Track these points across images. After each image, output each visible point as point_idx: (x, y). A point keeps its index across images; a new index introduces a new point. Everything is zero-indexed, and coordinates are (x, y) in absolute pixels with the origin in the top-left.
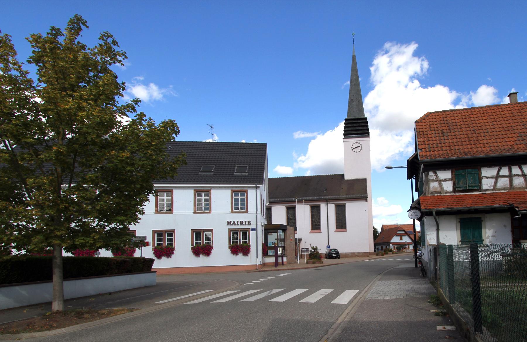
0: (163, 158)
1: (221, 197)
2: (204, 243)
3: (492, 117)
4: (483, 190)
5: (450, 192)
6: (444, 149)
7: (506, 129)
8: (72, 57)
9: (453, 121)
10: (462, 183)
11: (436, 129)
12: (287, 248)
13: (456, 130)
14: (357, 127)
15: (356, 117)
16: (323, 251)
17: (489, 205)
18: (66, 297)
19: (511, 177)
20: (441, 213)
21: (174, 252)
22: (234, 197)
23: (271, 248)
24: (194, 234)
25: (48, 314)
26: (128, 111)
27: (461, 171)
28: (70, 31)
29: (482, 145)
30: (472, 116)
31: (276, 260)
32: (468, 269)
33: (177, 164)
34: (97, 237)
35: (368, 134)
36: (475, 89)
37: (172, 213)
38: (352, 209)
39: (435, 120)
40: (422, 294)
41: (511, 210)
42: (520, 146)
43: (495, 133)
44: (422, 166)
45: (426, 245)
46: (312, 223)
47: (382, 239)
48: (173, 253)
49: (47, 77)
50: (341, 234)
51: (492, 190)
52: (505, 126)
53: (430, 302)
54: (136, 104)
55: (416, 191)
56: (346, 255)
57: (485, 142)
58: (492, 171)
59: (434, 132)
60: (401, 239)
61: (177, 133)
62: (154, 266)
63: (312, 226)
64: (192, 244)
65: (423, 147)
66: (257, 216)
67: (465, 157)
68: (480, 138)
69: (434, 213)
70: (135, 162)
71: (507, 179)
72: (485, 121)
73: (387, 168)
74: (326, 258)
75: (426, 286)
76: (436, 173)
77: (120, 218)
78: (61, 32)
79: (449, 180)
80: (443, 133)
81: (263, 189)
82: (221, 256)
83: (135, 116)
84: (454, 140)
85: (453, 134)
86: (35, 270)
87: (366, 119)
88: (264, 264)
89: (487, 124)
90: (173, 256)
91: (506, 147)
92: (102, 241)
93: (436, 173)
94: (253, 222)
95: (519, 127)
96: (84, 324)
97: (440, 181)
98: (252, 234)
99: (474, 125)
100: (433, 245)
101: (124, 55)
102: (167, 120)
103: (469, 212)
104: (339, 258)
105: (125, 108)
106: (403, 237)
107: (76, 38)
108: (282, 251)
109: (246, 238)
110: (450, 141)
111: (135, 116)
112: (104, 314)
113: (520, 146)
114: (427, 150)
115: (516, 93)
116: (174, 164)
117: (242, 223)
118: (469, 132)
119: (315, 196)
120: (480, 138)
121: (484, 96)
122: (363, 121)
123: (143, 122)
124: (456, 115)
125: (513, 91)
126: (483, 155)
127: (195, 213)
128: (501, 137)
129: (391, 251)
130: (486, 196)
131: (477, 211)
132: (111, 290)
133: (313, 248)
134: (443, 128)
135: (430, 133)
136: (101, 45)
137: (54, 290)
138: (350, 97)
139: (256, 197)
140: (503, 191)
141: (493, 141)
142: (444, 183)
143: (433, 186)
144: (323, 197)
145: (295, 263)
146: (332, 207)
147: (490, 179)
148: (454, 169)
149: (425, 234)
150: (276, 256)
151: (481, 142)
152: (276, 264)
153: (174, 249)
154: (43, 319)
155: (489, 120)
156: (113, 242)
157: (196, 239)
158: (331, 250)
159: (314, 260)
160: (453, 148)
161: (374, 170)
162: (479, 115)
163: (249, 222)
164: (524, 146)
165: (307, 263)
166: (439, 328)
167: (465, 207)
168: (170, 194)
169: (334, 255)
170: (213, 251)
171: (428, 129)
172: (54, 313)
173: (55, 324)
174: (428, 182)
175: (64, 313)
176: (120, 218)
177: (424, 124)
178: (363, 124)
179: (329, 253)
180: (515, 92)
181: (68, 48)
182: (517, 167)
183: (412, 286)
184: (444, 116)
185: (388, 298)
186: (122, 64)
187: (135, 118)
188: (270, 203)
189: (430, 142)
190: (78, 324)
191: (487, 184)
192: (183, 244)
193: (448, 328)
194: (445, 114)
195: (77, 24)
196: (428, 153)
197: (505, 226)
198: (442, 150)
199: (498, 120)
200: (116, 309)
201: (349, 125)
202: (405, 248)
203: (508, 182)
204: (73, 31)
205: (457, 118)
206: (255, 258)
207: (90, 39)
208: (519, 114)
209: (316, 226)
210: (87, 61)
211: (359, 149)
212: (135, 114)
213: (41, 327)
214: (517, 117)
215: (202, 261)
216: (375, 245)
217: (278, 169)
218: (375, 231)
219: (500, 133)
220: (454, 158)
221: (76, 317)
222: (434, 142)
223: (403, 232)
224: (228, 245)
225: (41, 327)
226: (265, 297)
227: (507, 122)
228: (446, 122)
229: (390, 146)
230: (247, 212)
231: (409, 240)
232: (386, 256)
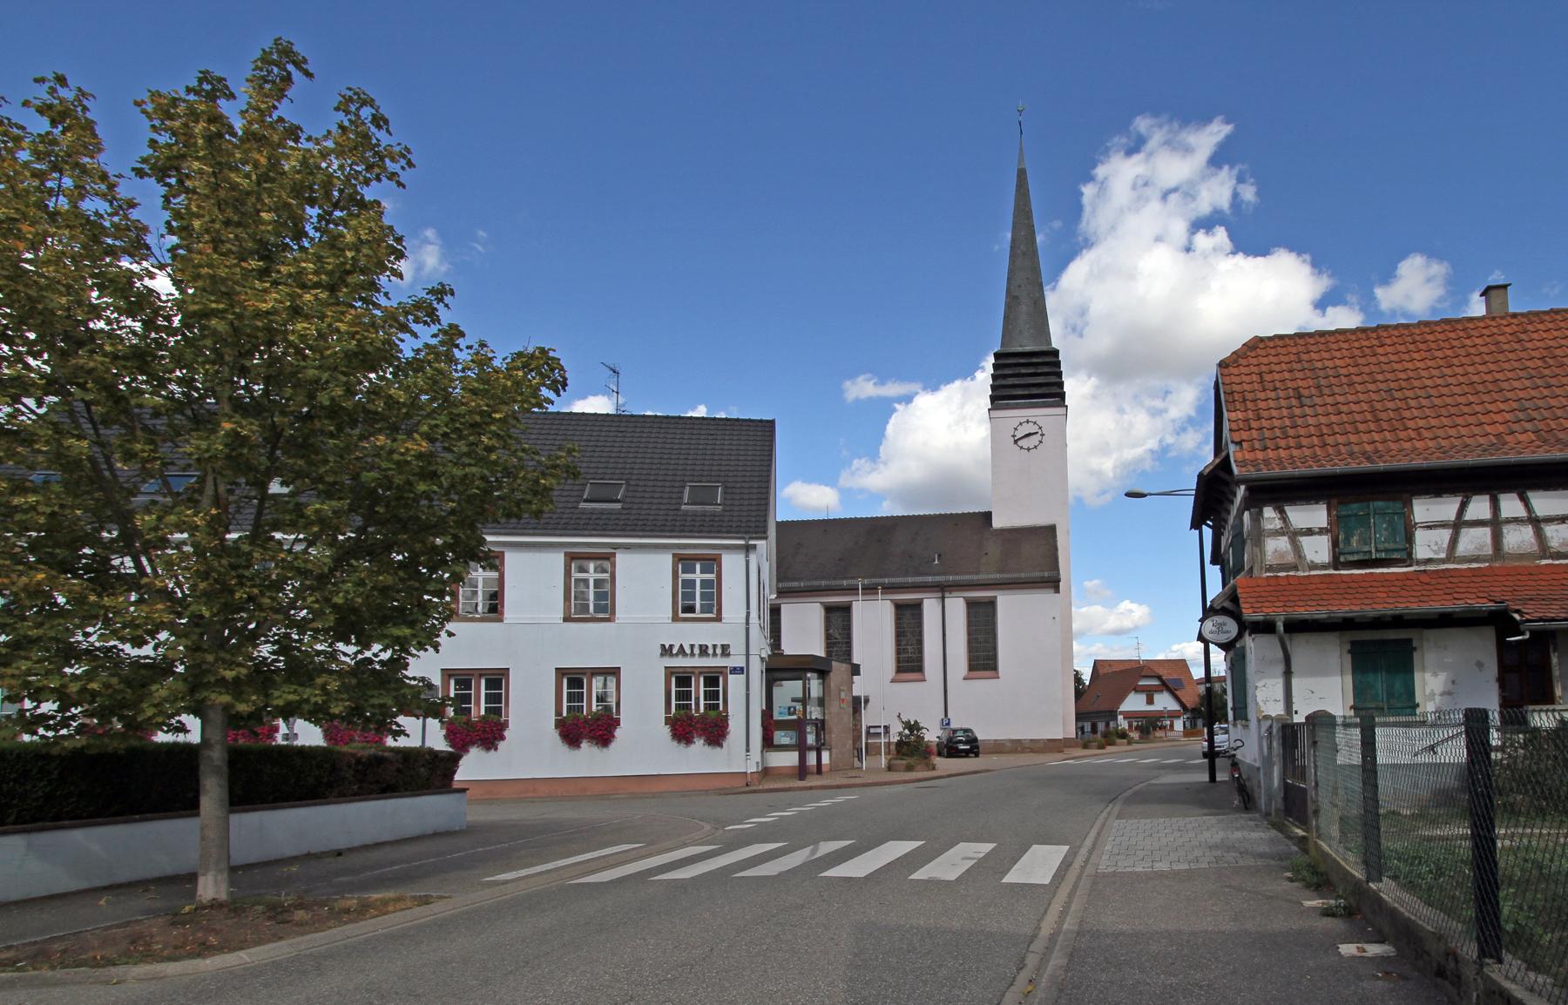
0: (520, 459)
1: (644, 575)
2: (594, 708)
3: (1439, 354)
4: (1419, 563)
5: (1324, 567)
6: (1304, 442)
7: (1480, 388)
8: (263, 161)
9: (1328, 363)
10: (1359, 542)
11: (1278, 385)
12: (830, 724)
13: (1337, 390)
14: (1028, 378)
15: (1028, 349)
16: (932, 735)
18: (233, 863)
19: (1496, 524)
20: (1298, 627)
21: (506, 733)
22: (683, 576)
23: (783, 725)
24: (565, 681)
25: (187, 909)
26: (417, 321)
27: (1355, 506)
28: (261, 87)
29: (1413, 434)
30: (1380, 350)
31: (802, 759)
33: (553, 476)
34: (334, 685)
35: (1062, 396)
36: (1388, 276)
37: (501, 620)
38: (1011, 608)
39: (1275, 360)
40: (1261, 856)
41: (1500, 621)
42: (1521, 438)
43: (1449, 400)
44: (1241, 491)
45: (1252, 715)
46: (898, 652)
47: (1101, 696)
48: (502, 738)
49: (207, 218)
50: (983, 686)
51: (1443, 561)
52: (1475, 378)
53: (1291, 880)
54: (441, 300)
55: (1213, 562)
56: (998, 748)
57: (1421, 423)
58: (1446, 508)
59: (1273, 395)
60: (1150, 701)
61: (560, 386)
62: (461, 775)
63: (898, 661)
64: (558, 712)
65: (1245, 435)
66: (747, 630)
67: (1366, 466)
68: (1407, 414)
69: (1280, 626)
70: (441, 469)
71: (1487, 531)
72: (1419, 364)
73: (1129, 495)
74: (940, 754)
76: (1282, 512)
77: (396, 632)
78: (227, 87)
79: (1321, 531)
80: (1299, 397)
81: (765, 548)
82: (644, 745)
83: (435, 336)
84: (1334, 418)
85: (1330, 400)
86: (121, 781)
87: (1056, 353)
88: (766, 772)
89: (1424, 373)
90: (502, 745)
91: (1482, 440)
92: (345, 696)
93: (1282, 512)
94: (737, 648)
95: (1516, 384)
96: (299, 939)
97: (1294, 535)
98: (735, 683)
99: (1389, 376)
100: (1278, 718)
101: (404, 157)
102: (530, 350)
103: (1378, 623)
104: (977, 755)
105: (407, 313)
106: (1157, 697)
107: (275, 108)
108: (818, 736)
109: (715, 695)
110: (1323, 420)
111: (435, 336)
112: (347, 911)
113: (1521, 438)
114: (1257, 445)
115: (1505, 287)
116: (544, 475)
117: (704, 651)
118: (1374, 397)
119: (906, 574)
120: (1407, 414)
121: (1414, 290)
122: (1047, 359)
123: (456, 351)
124: (1335, 346)
125: (1497, 278)
126: (1418, 462)
127: (566, 619)
128: (1466, 409)
129: (1123, 735)
130: (1425, 579)
131: (1398, 621)
132: (342, 843)
133: (908, 725)
134: (1300, 383)
135: (1262, 395)
136: (341, 127)
137: (203, 838)
138: (1008, 291)
139: (743, 574)
140: (1475, 565)
141: (1445, 421)
142: (1305, 541)
143: (1276, 547)
144: (930, 579)
145: (853, 768)
147: (1436, 530)
148: (1334, 501)
149: (1250, 685)
150: (802, 748)
151: (1411, 424)
152: (802, 771)
153: (505, 725)
154: (173, 924)
155: (1430, 363)
156: (376, 701)
157: (571, 698)
158: (955, 731)
159: (910, 761)
160: (1330, 440)
161: (1079, 500)
162: (1402, 348)
163: (725, 648)
165: (890, 768)
166: (1348, 949)
167: (1367, 608)
168: (607, 565)
169: (960, 746)
170: (618, 732)
171: (1256, 386)
172: (205, 908)
173: (212, 940)
174: (1259, 536)
175: (233, 907)
176: (396, 632)
177: (1243, 370)
178: (1046, 369)
179: (950, 740)
180: (1501, 283)
181: (254, 134)
182: (1514, 495)
183: (1221, 834)
184: (1301, 349)
185: (1163, 866)
186: (400, 184)
187: (434, 341)
188: (782, 593)
189: (1265, 423)
190: (281, 938)
191: (1428, 545)
192: (532, 710)
193: (1374, 950)
194: (1302, 342)
195: (279, 68)
196: (1260, 455)
197: (1480, 665)
198: (1300, 447)
199: (1455, 361)
200: (375, 896)
201: (1007, 371)
202: (1163, 728)
203: (1489, 540)
204: (268, 86)
205: (1338, 354)
206: (739, 754)
207: (312, 114)
208: (1516, 346)
209: (909, 662)
210: (311, 173)
211: (1034, 440)
212: (435, 329)
213: (176, 948)
214: (1511, 356)
215: (588, 762)
216: (1079, 717)
217: (803, 496)
218: (1078, 678)
219: (1462, 400)
220: (1297, 472)
221: (269, 918)
222: (1276, 423)
223: (1156, 682)
225: (176, 948)
227: (1481, 368)
228: (1306, 365)
229: (1120, 436)
230: (719, 619)
231: (1173, 706)
232: (1110, 749)
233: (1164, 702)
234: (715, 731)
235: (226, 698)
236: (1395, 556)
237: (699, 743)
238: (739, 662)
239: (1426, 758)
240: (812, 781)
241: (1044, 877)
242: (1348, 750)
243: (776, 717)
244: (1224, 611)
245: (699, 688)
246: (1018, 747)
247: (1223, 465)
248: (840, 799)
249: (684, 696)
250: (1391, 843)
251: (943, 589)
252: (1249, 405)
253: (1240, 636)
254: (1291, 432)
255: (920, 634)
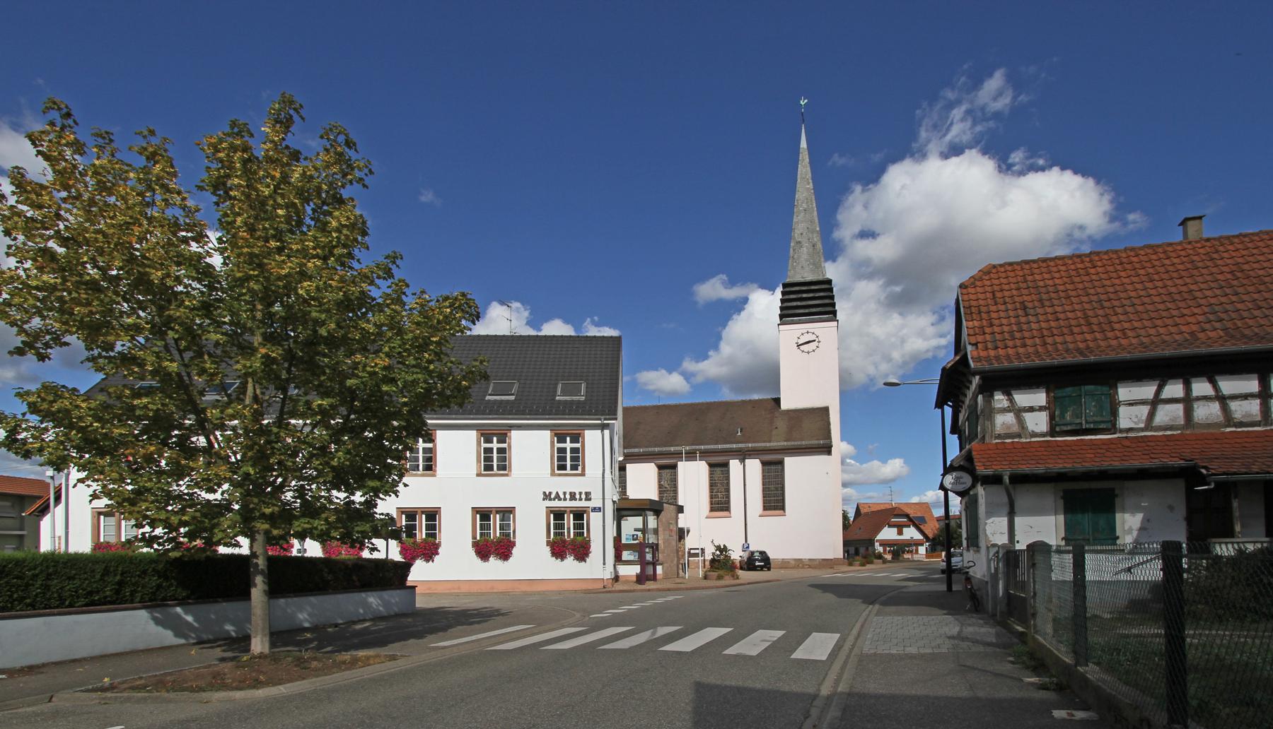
1: (531, 446)
4: (1121, 431)
10: (1072, 416)
17: (1136, 463)
19: (1188, 401)
20: (1020, 479)
23: (629, 547)
26: (379, 277)
31: (643, 570)
32: (1068, 596)
41: (1189, 475)
42: (1211, 334)
44: (976, 380)
45: (982, 544)
46: (711, 497)
50: (774, 521)
51: (1142, 430)
55: (953, 432)
56: (785, 564)
57: (1126, 325)
58: (1147, 391)
59: (1003, 307)
60: (900, 533)
64: (474, 537)
65: (980, 338)
68: (1114, 319)
74: (742, 568)
75: (992, 631)
79: (1041, 409)
90: (437, 558)
93: (1009, 394)
97: (1019, 412)
98: (595, 519)
104: (769, 569)
113: (1211, 334)
114: (990, 345)
127: (478, 475)
129: (880, 556)
130: (1128, 444)
131: (1103, 475)
133: (718, 548)
140: (1169, 433)
143: (1004, 421)
144: (734, 446)
146: (754, 466)
147: (1134, 405)
149: (981, 523)
152: (641, 579)
158: (752, 553)
159: (721, 572)
163: (588, 494)
164: (1222, 333)
165: (705, 577)
166: (1059, 714)
170: (514, 551)
174: (990, 413)
179: (749, 559)
185: (912, 650)
186: (364, 186)
188: (626, 455)
191: (1129, 418)
192: (456, 534)
193: (1080, 715)
197: (1171, 508)
198: (1024, 346)
199: (1156, 277)
206: (597, 567)
209: (720, 503)
215: (495, 570)
216: (846, 544)
220: (1056, 362)
224: (545, 540)
226: (647, 642)
230: (583, 474)
231: (918, 536)
232: (868, 566)
233: (911, 533)
234: (581, 551)
235: (266, 526)
236: (1101, 426)
237: (570, 560)
238: (596, 502)
239: (1124, 577)
240: (650, 585)
241: (822, 655)
242: (1062, 569)
243: (624, 541)
244: (961, 468)
245: (569, 521)
246: (799, 564)
247: (964, 361)
248: (671, 598)
249: (559, 527)
250: (1095, 639)
251: (743, 455)
252: (984, 316)
253: (973, 486)
254: (1018, 335)
255: (728, 484)
